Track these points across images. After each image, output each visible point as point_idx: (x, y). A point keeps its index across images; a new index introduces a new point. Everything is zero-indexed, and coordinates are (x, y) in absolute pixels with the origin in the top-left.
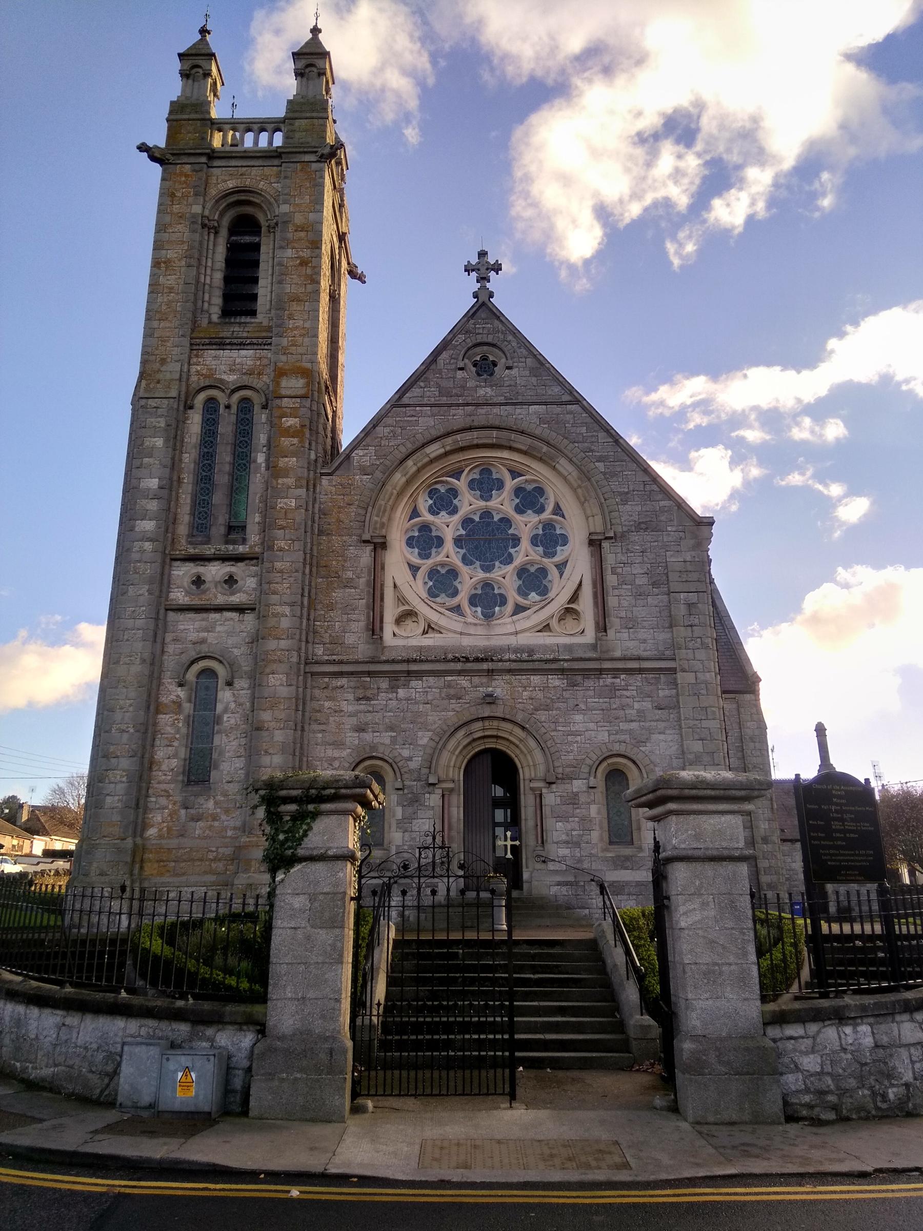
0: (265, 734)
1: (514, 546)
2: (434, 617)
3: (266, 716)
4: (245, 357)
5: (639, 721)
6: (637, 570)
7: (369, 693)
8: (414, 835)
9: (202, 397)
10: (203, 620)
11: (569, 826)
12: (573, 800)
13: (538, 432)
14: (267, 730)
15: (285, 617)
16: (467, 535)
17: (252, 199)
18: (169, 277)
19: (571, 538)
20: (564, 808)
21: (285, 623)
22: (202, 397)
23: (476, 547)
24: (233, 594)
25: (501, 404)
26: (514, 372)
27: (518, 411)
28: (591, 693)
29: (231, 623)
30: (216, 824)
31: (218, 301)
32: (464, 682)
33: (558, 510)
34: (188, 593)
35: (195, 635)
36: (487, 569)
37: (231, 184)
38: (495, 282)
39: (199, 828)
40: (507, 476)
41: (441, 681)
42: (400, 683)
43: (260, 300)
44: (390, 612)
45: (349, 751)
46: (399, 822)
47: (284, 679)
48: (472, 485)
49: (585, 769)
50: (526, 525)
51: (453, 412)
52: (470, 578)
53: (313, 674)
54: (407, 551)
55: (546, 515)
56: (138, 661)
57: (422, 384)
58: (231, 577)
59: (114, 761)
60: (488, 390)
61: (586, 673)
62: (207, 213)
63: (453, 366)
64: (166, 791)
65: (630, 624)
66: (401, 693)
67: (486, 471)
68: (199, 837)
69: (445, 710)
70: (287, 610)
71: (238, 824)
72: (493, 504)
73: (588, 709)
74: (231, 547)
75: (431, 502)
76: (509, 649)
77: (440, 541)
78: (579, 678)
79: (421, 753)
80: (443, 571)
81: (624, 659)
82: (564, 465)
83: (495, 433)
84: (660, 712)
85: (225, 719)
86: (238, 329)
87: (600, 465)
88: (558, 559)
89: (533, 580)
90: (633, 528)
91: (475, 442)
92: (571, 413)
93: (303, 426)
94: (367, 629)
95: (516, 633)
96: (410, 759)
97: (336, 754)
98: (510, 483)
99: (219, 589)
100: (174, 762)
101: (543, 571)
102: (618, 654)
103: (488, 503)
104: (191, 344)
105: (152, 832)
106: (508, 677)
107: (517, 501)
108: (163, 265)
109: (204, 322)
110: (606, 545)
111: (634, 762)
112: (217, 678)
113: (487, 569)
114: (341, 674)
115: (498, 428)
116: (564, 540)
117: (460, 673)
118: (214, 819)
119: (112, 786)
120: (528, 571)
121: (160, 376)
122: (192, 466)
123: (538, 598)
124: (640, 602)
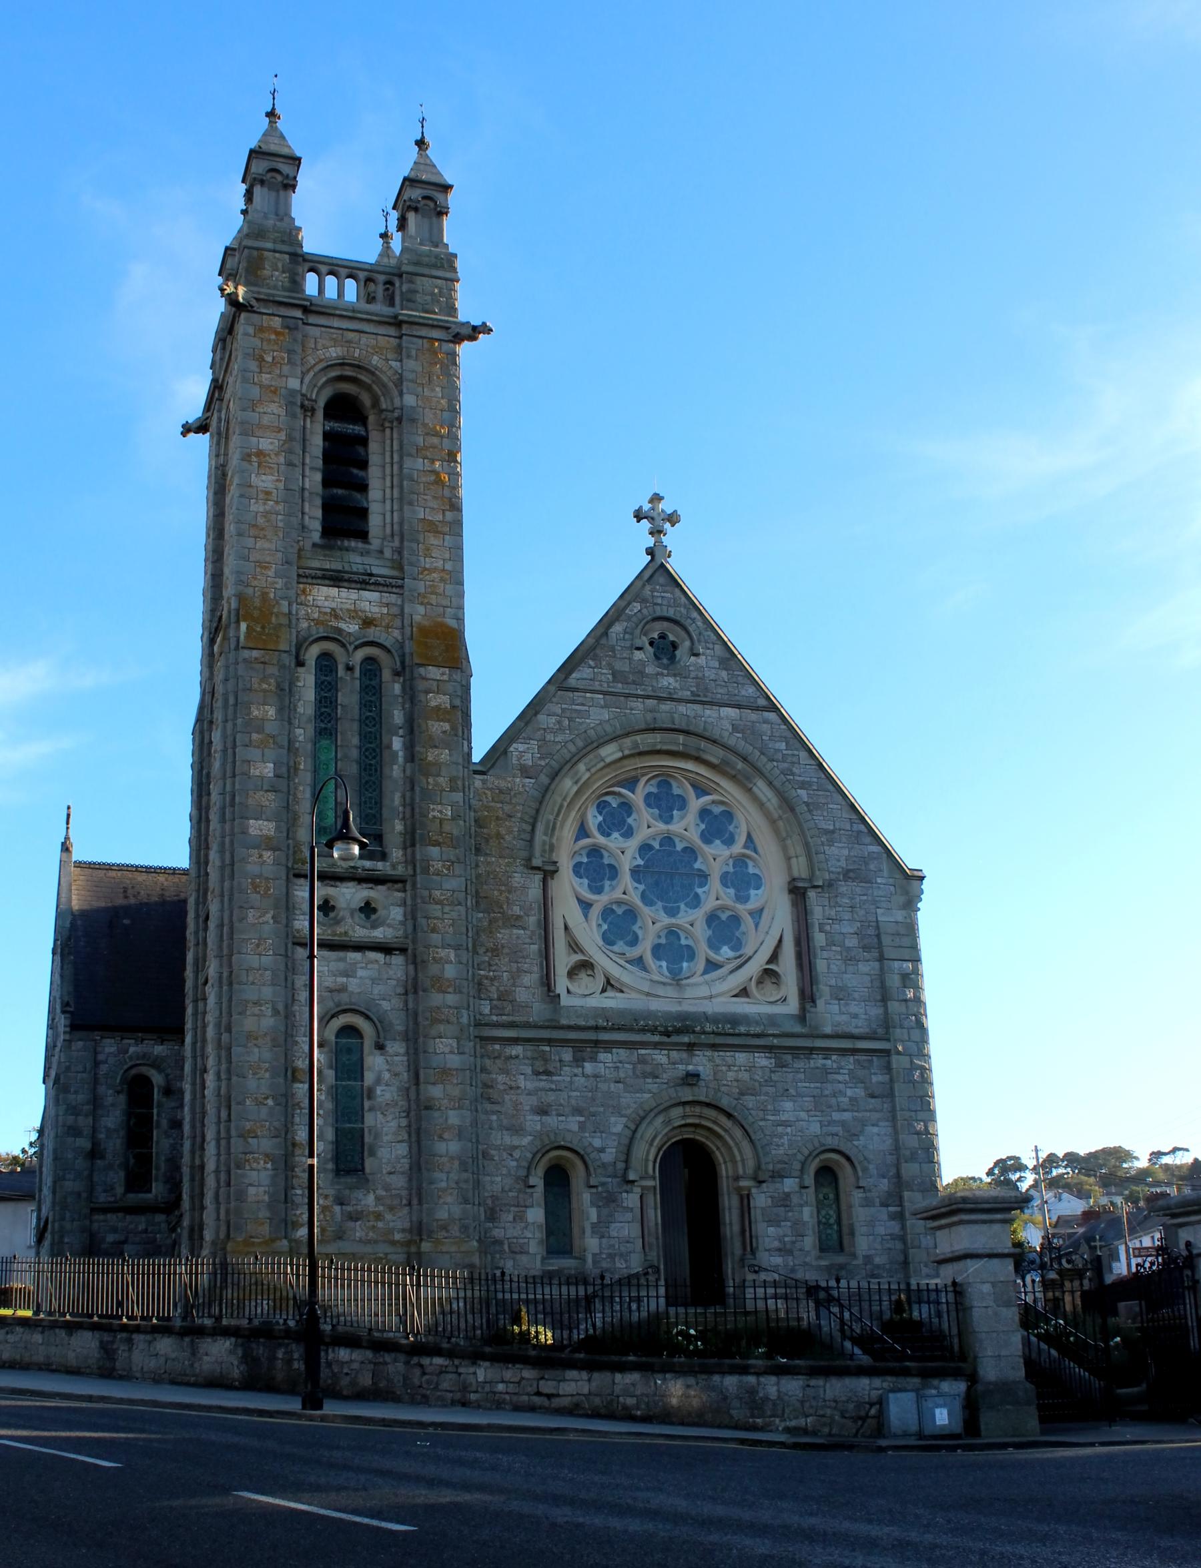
0: (437, 1114)
1: (701, 885)
2: (615, 971)
3: (436, 1091)
4: (370, 601)
5: (853, 1111)
6: (847, 929)
8: (612, 1242)
9: (314, 651)
11: (780, 1231)
12: (784, 1201)
13: (732, 742)
14: (439, 1109)
16: (646, 866)
17: (359, 376)
18: (264, 477)
20: (775, 1210)
23: (657, 884)
24: (374, 926)
26: (702, 660)
27: (708, 712)
28: (802, 1076)
29: (376, 966)
30: (380, 1224)
32: (660, 1057)
33: (750, 841)
35: (331, 979)
36: (672, 912)
37: (334, 352)
38: (672, 538)
39: (358, 1230)
40: (741, 839)
44: (563, 960)
45: (530, 1138)
46: (594, 1226)
47: (455, 1045)
50: (716, 857)
51: (633, 704)
53: (482, 1039)
54: (576, 881)
56: (269, 1012)
57: (591, 663)
58: (368, 904)
60: (671, 680)
61: (795, 1051)
63: (628, 644)
65: (841, 994)
66: (589, 1067)
67: (665, 784)
68: (361, 1241)
69: (642, 1091)
71: (407, 1225)
72: (676, 827)
75: (600, 818)
77: (613, 872)
79: (616, 1143)
80: (620, 911)
83: (681, 738)
84: (873, 1100)
85: (378, 1092)
86: (355, 559)
87: (803, 793)
88: (752, 905)
89: (724, 928)
90: (841, 877)
91: (658, 747)
92: (766, 721)
93: (453, 707)
94: (542, 984)
97: (516, 1141)
98: (696, 804)
99: (357, 919)
101: (736, 919)
102: (828, 1030)
104: (299, 576)
106: (708, 1053)
107: (703, 826)
108: (254, 459)
110: (812, 894)
111: (848, 1159)
112: (361, 1037)
113: (672, 912)
114: (515, 1041)
115: (687, 732)
116: (757, 882)
117: (656, 1045)
119: (255, 1173)
120: (719, 918)
123: (731, 954)
124: (850, 968)
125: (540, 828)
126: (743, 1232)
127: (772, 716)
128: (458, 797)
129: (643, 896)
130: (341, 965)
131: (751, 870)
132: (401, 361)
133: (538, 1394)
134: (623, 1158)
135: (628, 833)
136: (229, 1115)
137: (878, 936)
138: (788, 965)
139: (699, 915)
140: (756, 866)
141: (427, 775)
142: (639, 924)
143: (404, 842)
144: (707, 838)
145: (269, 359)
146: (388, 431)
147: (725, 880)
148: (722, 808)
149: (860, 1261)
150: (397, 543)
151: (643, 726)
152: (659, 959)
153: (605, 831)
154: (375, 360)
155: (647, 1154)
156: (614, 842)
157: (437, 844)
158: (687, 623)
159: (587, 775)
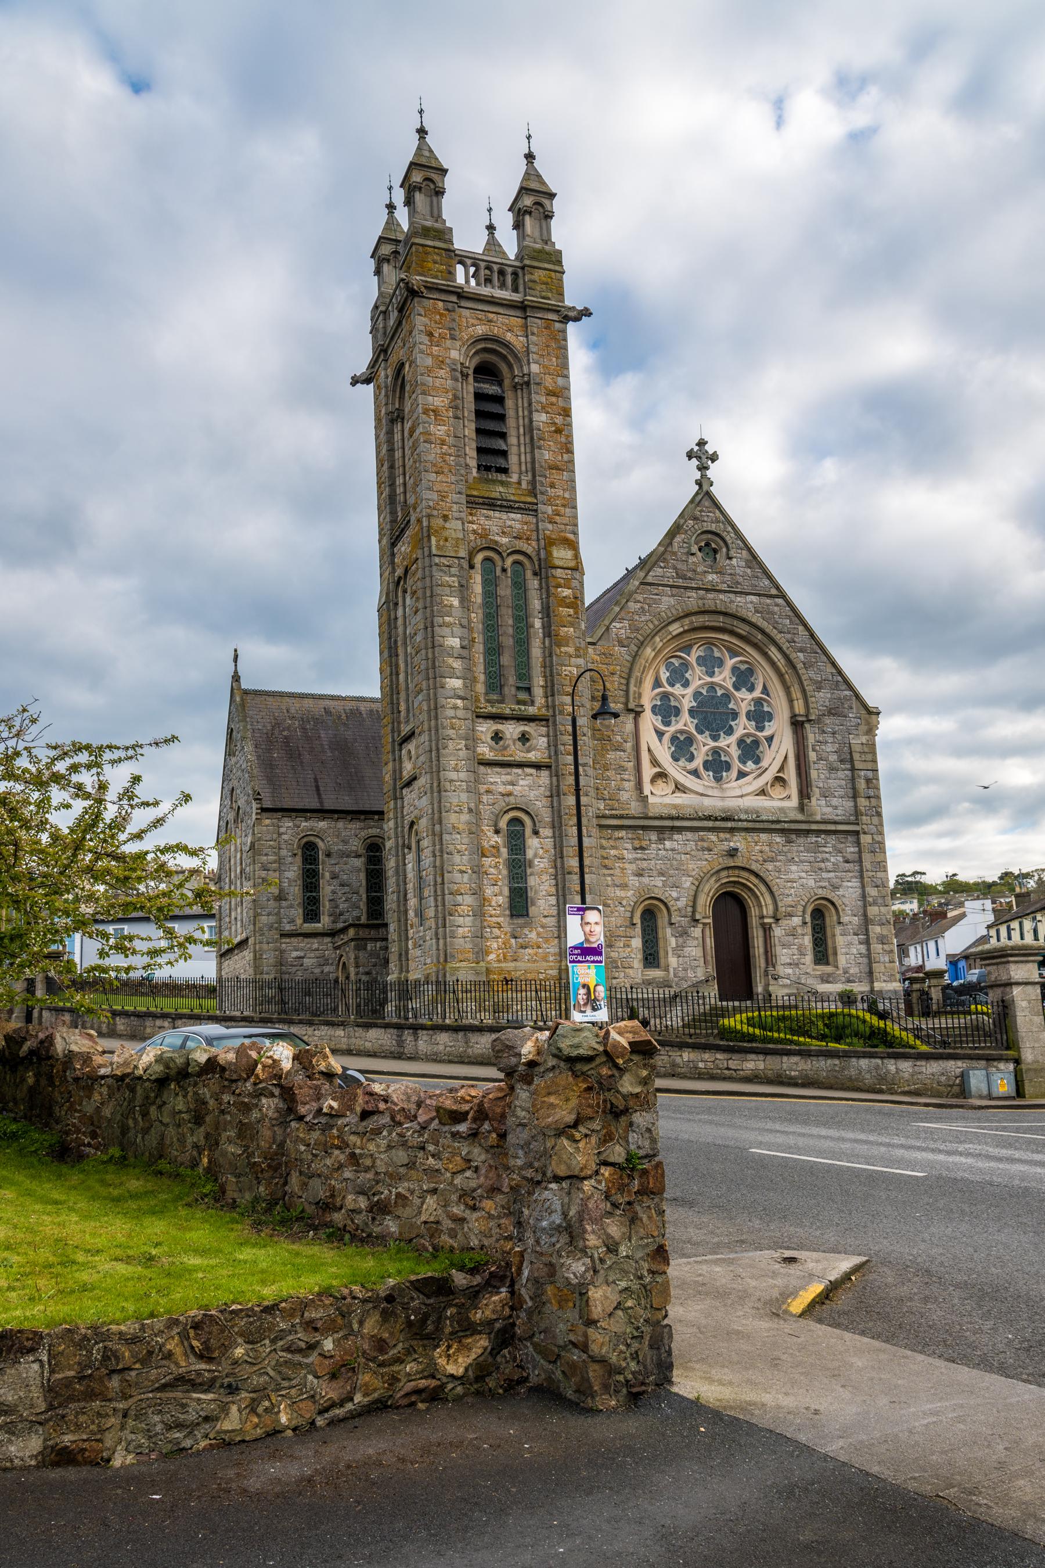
1: (734, 720)
4: (515, 521)
7: (644, 844)
9: (480, 557)
10: (508, 774)
13: (754, 620)
16: (698, 707)
19: (775, 716)
22: (480, 557)
24: (528, 751)
25: (725, 592)
27: (739, 599)
30: (540, 950)
32: (713, 837)
34: (491, 748)
37: (480, 330)
38: (714, 471)
40: (759, 688)
41: (695, 836)
42: (666, 836)
44: (648, 771)
46: (674, 949)
50: (744, 700)
51: (690, 594)
57: (662, 565)
58: (523, 735)
59: (459, 898)
60: (715, 576)
61: (798, 832)
64: (498, 923)
73: (802, 862)
74: (523, 708)
78: (794, 836)
87: (801, 655)
88: (767, 733)
89: (750, 750)
92: (777, 605)
94: (637, 789)
95: (742, 796)
96: (677, 899)
98: (730, 663)
100: (500, 899)
102: (818, 818)
103: (735, 692)
110: (807, 725)
111: (833, 904)
112: (523, 826)
113: (715, 738)
116: (770, 717)
118: (539, 947)
121: (446, 533)
122: (481, 626)
123: (754, 766)
125: (632, 681)
126: (766, 952)
127: (780, 601)
129: (697, 728)
130: (509, 778)
131: (766, 709)
132: (527, 336)
133: (728, 1069)
134: (691, 904)
135: (686, 684)
136: (443, 880)
137: (851, 753)
139: (733, 739)
141: (559, 646)
142: (695, 746)
143: (546, 693)
145: (437, 335)
146: (519, 391)
147: (749, 716)
148: (746, 666)
150: (530, 477)
151: (696, 609)
152: (708, 771)
154: (509, 337)
155: (705, 903)
156: (677, 690)
158: (724, 534)
159: (661, 644)
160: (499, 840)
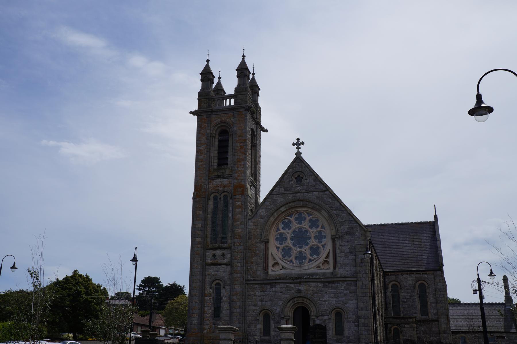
2: (284, 264)
3: (234, 297)
4: (225, 181)
9: (212, 195)
15: (238, 266)
21: (239, 269)
22: (212, 195)
31: (216, 161)
32: (292, 286)
33: (323, 227)
34: (211, 259)
37: (218, 120)
43: (229, 160)
44: (271, 263)
48: (296, 219)
49: (328, 312)
50: (313, 232)
52: (295, 250)
53: (248, 284)
55: (319, 229)
58: (223, 254)
61: (329, 282)
62: (211, 132)
70: (239, 265)
76: (306, 274)
77: (286, 239)
78: (327, 284)
81: (340, 277)
82: (323, 212)
87: (335, 212)
89: (315, 251)
93: (242, 205)
95: (309, 269)
98: (308, 218)
100: (210, 311)
101: (318, 248)
102: (339, 276)
105: (205, 331)
109: (212, 170)
113: (307, 244)
114: (256, 284)
116: (325, 237)
117: (291, 283)
127: (327, 192)
128: (243, 226)
138: (331, 259)
140: (324, 232)
144: (311, 227)
147: (315, 238)
149: (346, 338)
153: (284, 229)
154: (228, 120)
157: (237, 238)
160: (211, 291)
